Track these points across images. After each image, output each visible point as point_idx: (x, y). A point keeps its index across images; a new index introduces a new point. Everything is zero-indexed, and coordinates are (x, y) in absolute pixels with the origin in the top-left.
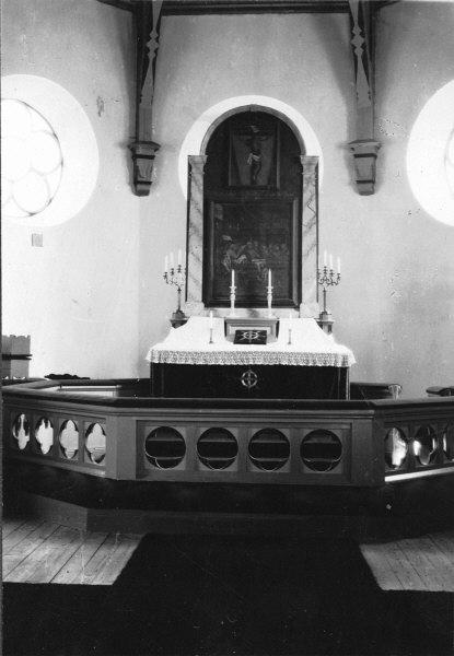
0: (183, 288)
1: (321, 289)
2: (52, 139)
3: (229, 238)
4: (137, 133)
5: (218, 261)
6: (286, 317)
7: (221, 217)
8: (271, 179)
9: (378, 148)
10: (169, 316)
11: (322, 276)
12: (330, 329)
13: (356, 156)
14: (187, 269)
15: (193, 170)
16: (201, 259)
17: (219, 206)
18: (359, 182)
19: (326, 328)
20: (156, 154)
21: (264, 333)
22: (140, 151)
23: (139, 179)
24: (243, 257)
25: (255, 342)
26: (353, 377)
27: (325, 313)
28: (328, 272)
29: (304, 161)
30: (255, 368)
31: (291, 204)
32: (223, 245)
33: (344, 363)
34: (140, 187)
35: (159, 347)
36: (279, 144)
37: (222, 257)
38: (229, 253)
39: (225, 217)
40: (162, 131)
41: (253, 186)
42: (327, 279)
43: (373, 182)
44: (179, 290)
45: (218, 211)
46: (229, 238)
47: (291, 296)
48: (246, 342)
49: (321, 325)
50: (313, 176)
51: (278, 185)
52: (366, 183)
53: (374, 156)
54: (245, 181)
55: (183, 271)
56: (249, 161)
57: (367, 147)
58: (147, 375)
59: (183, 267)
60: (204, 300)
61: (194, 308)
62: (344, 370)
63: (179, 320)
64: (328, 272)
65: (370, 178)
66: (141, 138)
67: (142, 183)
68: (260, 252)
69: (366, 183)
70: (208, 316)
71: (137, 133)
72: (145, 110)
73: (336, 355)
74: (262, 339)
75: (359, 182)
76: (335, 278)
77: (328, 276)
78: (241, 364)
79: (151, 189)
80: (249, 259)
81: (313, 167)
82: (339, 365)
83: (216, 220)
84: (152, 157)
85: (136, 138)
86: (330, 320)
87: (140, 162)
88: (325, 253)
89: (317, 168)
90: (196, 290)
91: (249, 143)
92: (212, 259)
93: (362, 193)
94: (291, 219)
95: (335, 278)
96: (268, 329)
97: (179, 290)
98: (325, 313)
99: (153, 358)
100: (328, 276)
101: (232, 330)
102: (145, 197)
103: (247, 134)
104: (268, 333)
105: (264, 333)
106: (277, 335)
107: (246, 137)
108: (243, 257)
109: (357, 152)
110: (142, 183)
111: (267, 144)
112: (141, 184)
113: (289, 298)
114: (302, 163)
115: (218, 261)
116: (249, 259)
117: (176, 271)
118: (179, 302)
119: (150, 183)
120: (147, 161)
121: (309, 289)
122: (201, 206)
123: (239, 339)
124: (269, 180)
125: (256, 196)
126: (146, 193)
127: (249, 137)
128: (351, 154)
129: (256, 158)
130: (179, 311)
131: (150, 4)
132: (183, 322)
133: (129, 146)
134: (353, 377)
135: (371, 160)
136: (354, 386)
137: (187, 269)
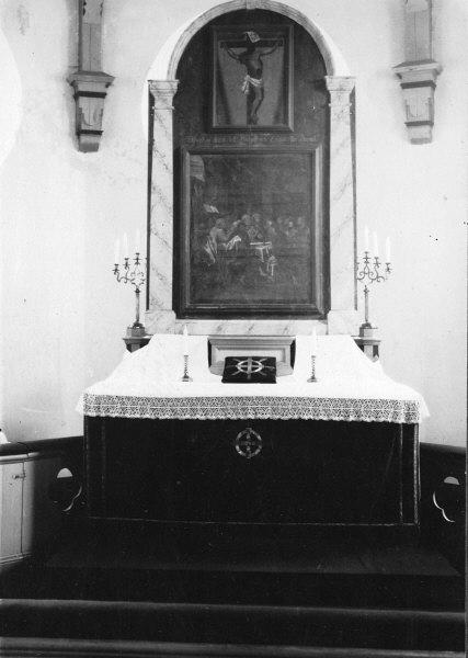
0: (143, 289)
1: (361, 288)
3: (214, 209)
4: (80, 61)
5: (195, 244)
6: (303, 331)
7: (200, 177)
8: (281, 114)
9: (437, 73)
10: (123, 332)
11: (361, 267)
12: (376, 352)
13: (405, 86)
14: (148, 259)
15: (158, 104)
17: (198, 160)
18: (409, 124)
19: (369, 349)
21: (271, 362)
23: (84, 127)
24: (237, 239)
25: (256, 378)
26: (422, 436)
27: (367, 325)
28: (372, 261)
29: (332, 84)
30: (257, 424)
31: (312, 155)
32: (208, 220)
33: (408, 415)
34: (85, 139)
35: (99, 389)
36: (291, 63)
37: (204, 238)
38: (215, 232)
39: (208, 174)
40: (115, 61)
41: (253, 128)
42: (369, 270)
43: (430, 123)
44: (138, 292)
45: (195, 167)
46: (214, 209)
47: (312, 299)
48: (242, 378)
49: (361, 344)
50: (347, 110)
51: (291, 124)
52: (419, 125)
53: (431, 84)
54: (239, 119)
55: (143, 261)
56: (245, 87)
57: (422, 72)
58: (77, 430)
59: (143, 256)
61: (162, 316)
62: (410, 429)
63: (137, 340)
64: (372, 261)
65: (426, 118)
66: (85, 67)
67: (87, 132)
68: (265, 232)
69: (419, 125)
70: (181, 333)
71: (80, 61)
73: (395, 403)
74: (268, 375)
75: (409, 124)
76: (382, 271)
77: (371, 266)
78: (234, 417)
79: (102, 141)
80: (246, 241)
81: (347, 96)
82: (401, 420)
83: (194, 181)
84: (103, 95)
85: (80, 66)
86: (374, 337)
87: (83, 101)
88: (367, 231)
89: (353, 95)
90: (163, 292)
91: (244, 59)
92: (187, 243)
93: (414, 141)
94: (312, 176)
95: (382, 271)
96: (279, 357)
97: (138, 292)
98: (367, 325)
99: (87, 408)
100: (371, 266)
101: (221, 356)
102: (94, 154)
103: (239, 45)
104: (278, 359)
105: (271, 362)
106: (292, 365)
107: (238, 51)
108: (237, 239)
109: (406, 80)
110: (87, 132)
111: (273, 60)
112: (86, 135)
113: (313, 306)
114: (329, 88)
115: (195, 244)
116: (246, 241)
117: (132, 262)
118: (138, 309)
119: (99, 133)
120: (94, 100)
121: (341, 289)
122: (169, 160)
123: (231, 373)
124: (277, 117)
125: (256, 142)
126: (94, 148)
127: (244, 50)
128: (397, 84)
129: (256, 82)
130: (137, 324)
131: (462, 609)
132: (144, 343)
133: (68, 81)
134: (422, 436)
135: (427, 90)
136: (429, 451)
137: (148, 259)
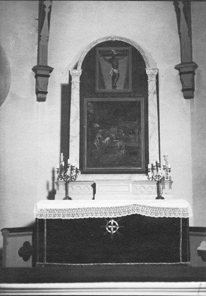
2: (92, 190)
7: (92, 111)
16: (79, 89)
20: (50, 74)
22: (40, 72)
23: (39, 90)
26: (191, 224)
34: (40, 95)
43: (193, 89)
46: (98, 125)
56: (111, 73)
60: (25, 260)
62: (186, 221)
72: (43, 46)
79: (48, 96)
84: (48, 76)
87: (40, 78)
102: (44, 102)
107: (108, 58)
108: (108, 139)
126: (43, 100)
127: (111, 57)
129: (116, 71)
135: (190, 75)
